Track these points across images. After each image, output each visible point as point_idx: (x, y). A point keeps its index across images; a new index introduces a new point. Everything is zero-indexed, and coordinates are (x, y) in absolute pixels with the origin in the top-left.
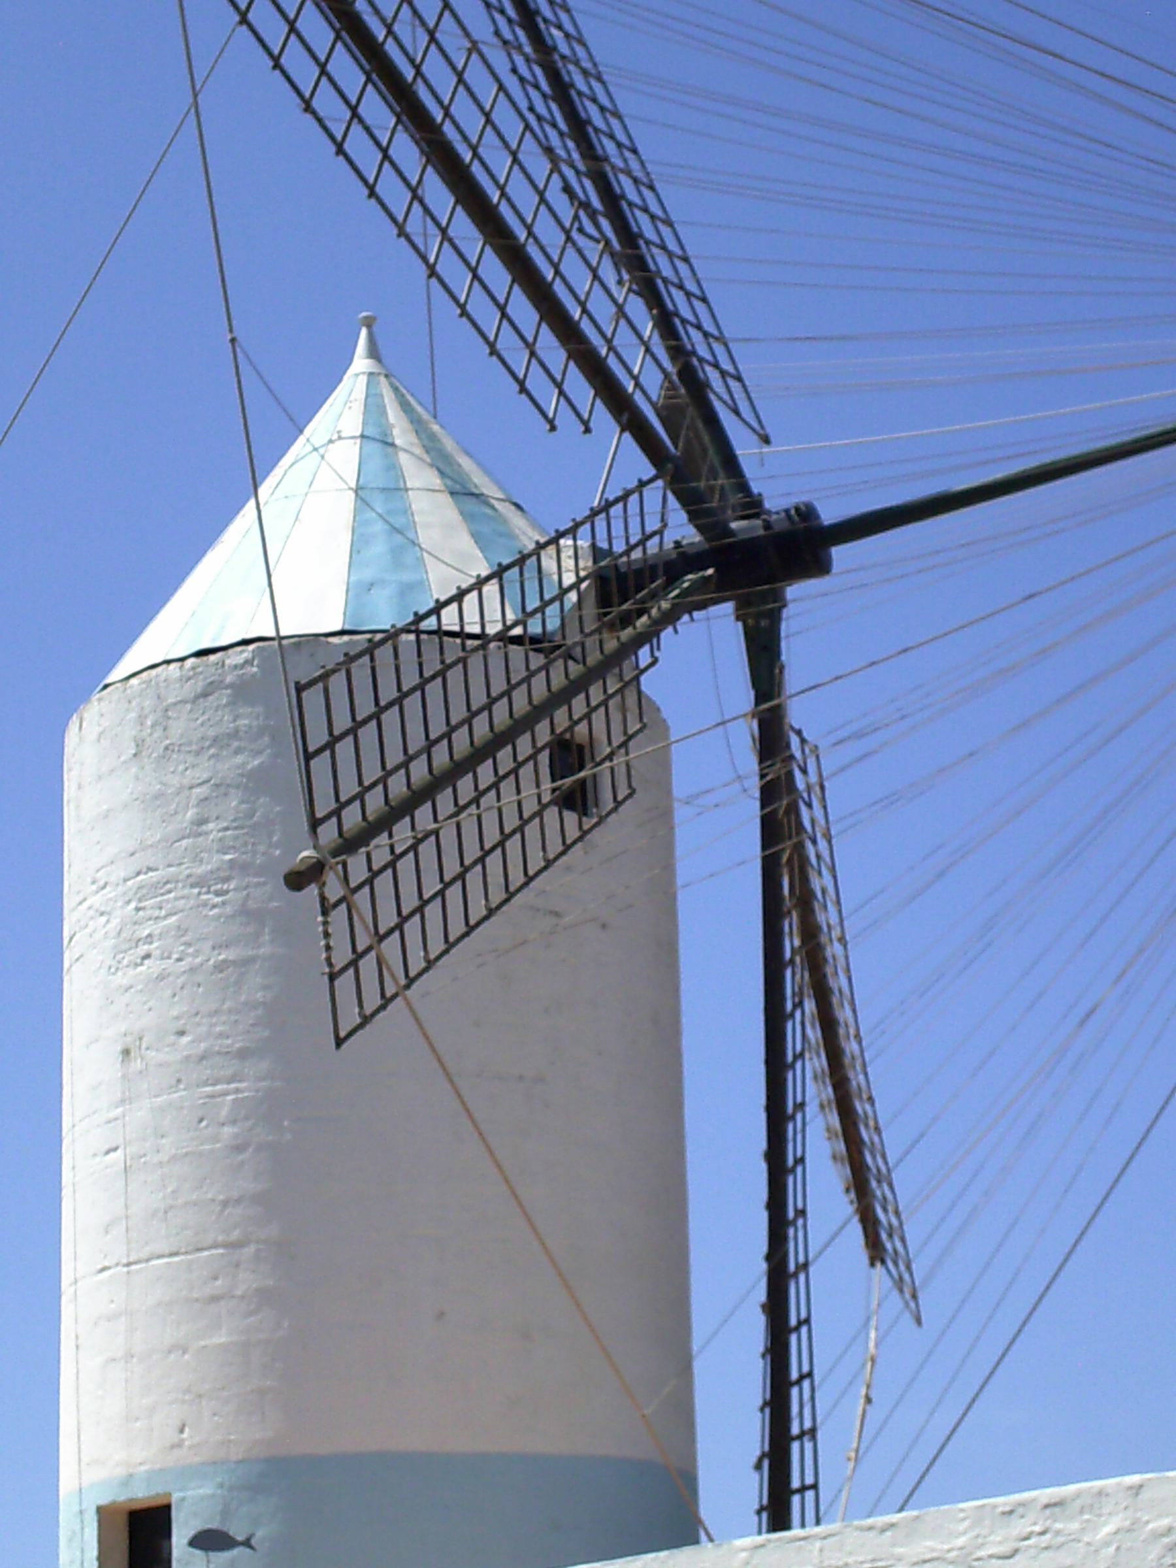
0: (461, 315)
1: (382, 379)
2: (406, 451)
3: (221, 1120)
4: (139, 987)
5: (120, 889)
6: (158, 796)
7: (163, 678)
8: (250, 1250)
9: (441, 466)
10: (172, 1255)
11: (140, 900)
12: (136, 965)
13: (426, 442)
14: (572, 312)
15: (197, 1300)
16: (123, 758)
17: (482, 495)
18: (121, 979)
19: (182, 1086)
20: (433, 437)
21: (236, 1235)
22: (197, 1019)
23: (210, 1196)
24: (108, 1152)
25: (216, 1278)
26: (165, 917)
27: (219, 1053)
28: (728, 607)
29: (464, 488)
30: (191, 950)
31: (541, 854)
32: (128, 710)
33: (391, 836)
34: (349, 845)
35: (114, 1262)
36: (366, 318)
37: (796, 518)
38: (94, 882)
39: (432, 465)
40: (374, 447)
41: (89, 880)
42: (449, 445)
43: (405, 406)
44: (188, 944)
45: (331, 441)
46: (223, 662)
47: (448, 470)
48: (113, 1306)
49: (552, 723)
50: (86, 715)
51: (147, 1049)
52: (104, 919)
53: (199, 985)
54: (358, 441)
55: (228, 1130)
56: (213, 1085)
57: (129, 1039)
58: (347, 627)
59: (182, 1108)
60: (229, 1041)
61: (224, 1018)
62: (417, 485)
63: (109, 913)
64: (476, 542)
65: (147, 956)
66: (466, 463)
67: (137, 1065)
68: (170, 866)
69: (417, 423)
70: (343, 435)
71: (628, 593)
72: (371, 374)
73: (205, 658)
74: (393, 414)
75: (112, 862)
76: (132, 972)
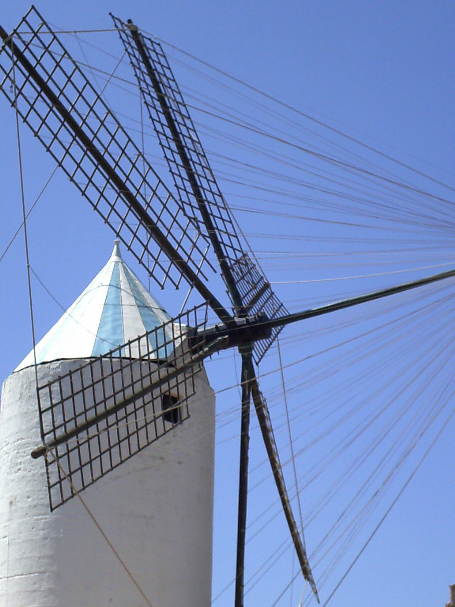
0: (128, 250)
1: (120, 264)
2: (124, 290)
3: (40, 528)
4: (17, 480)
5: (13, 445)
6: (26, 413)
7: (30, 371)
8: (48, 574)
9: (136, 296)
10: (21, 575)
11: (18, 449)
12: (16, 472)
13: (132, 287)
14: (173, 246)
15: (28, 591)
16: (16, 399)
17: (150, 307)
18: (11, 477)
19: (28, 516)
20: (135, 285)
21: (42, 569)
22: (34, 492)
23: (35, 555)
24: (4, 537)
25: (35, 584)
26: (26, 456)
27: (41, 505)
28: (236, 348)
29: (143, 304)
30: (33, 468)
31: (146, 440)
32: (18, 382)
33: (77, 437)
34: (56, 442)
35: (4, 576)
36: (116, 241)
37: (257, 318)
38: (5, 442)
39: (132, 296)
40: (113, 289)
41: (4, 441)
42: (141, 288)
43: (127, 274)
44: (33, 466)
45: (99, 287)
46: (50, 367)
47: (138, 298)
48: (2, 592)
49: (152, 394)
50: (6, 383)
51: (18, 502)
52: (7, 455)
53: (35, 480)
54: (108, 287)
55: (42, 532)
56: (38, 516)
57: (12, 498)
58: (93, 356)
59: (27, 524)
60: (44, 501)
61: (42, 493)
62: (127, 303)
63: (9, 453)
64: (144, 325)
65: (19, 469)
66: (146, 295)
67: (14, 508)
68: (28, 438)
69: (130, 280)
70: (103, 284)
71: (200, 343)
72: (116, 262)
73: (43, 365)
74: (122, 277)
75: (10, 435)
76: (14, 474)
